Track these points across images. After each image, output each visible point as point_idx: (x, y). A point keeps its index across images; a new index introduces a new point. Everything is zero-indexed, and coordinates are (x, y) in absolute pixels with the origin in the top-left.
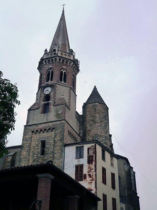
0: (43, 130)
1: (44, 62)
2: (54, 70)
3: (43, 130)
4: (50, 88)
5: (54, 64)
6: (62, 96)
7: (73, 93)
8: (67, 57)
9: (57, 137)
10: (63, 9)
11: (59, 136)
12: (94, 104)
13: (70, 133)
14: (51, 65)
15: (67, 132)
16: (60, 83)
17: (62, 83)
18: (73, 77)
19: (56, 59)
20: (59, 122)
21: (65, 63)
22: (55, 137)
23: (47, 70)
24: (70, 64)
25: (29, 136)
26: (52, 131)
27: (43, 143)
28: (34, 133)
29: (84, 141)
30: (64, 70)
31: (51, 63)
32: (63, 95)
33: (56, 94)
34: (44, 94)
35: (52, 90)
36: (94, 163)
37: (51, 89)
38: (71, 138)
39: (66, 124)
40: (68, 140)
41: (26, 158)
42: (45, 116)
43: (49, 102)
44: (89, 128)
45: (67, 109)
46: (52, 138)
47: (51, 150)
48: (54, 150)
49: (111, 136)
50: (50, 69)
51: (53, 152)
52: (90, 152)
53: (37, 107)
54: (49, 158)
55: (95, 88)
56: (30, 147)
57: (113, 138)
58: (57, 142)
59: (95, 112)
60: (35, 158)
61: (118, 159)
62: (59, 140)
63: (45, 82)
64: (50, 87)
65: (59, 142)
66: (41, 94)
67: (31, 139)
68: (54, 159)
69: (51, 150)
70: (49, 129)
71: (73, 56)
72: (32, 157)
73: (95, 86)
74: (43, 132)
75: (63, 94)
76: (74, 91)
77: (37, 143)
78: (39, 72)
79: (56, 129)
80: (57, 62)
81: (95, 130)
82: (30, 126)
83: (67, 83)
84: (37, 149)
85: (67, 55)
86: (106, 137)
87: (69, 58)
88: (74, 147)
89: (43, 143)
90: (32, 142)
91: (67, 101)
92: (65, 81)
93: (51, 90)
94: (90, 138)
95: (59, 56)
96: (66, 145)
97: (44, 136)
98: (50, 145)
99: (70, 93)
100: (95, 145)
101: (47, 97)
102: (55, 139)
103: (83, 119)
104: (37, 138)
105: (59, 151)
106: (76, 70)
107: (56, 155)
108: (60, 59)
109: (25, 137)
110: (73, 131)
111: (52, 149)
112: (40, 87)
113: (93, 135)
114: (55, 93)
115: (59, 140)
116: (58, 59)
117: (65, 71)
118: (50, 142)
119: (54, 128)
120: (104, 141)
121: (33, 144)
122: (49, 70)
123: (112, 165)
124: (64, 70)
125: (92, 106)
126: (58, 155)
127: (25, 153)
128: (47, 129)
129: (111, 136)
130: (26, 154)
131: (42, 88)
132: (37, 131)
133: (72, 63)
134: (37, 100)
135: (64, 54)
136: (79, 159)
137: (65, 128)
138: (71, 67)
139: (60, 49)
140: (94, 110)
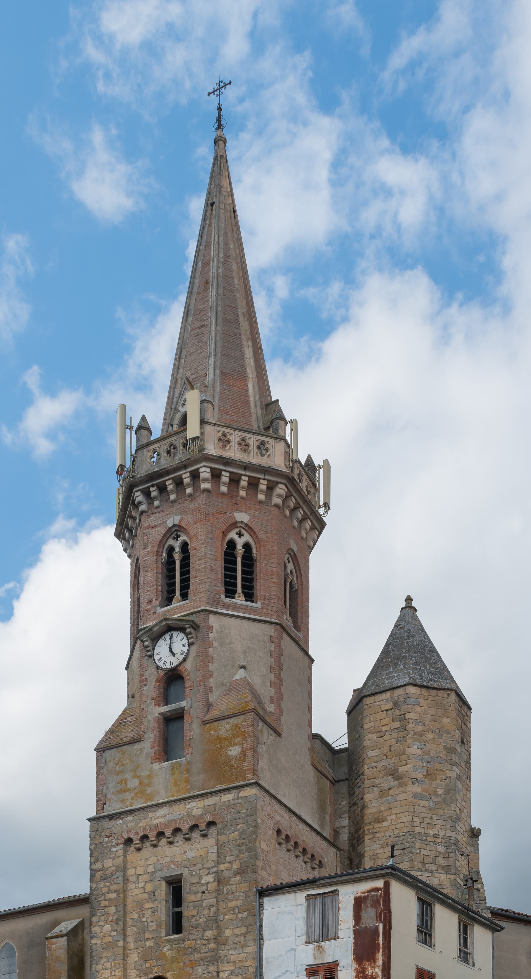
0: (168, 832)
1: (139, 497)
2: (190, 539)
3: (168, 832)
4: (181, 635)
5: (192, 506)
6: (241, 674)
7: (295, 647)
8: (254, 458)
9: (228, 859)
10: (219, 120)
11: (236, 856)
12: (397, 692)
13: (283, 837)
14: (174, 509)
15: (271, 833)
16: (226, 606)
17: (235, 607)
18: (290, 566)
19: (195, 475)
20: (228, 797)
21: (243, 493)
22: (218, 862)
23: (161, 543)
24: (271, 499)
25: (114, 859)
26: (204, 836)
27: (176, 888)
28: (132, 849)
29: (352, 866)
30: (240, 535)
31: (174, 502)
32: (243, 667)
33: (211, 667)
34: (158, 668)
35: (191, 644)
36: (380, 956)
37: (185, 641)
38: (294, 858)
39: (266, 805)
40: (284, 866)
41: (110, 946)
42: (175, 770)
43: (183, 704)
44: (371, 811)
45: (267, 736)
46: (210, 865)
47: (206, 912)
48: (216, 914)
49: (475, 834)
50: (175, 531)
51: (216, 921)
52: (364, 915)
53: (132, 735)
54: (204, 942)
55: (409, 606)
56: (125, 905)
57: (484, 843)
58: (229, 878)
59: (402, 734)
60: (150, 944)
61: (495, 929)
62: (237, 873)
63: (155, 607)
64: (182, 629)
65: (237, 879)
66: (142, 668)
67: (125, 870)
68: (222, 947)
69: (206, 912)
70: (194, 827)
71: (282, 443)
72: (137, 940)
73: (409, 599)
74: (171, 843)
75: (243, 663)
76: (300, 635)
77: (149, 887)
78: (125, 550)
79: (219, 826)
80: (205, 490)
81: (393, 815)
82: (111, 817)
83: (258, 605)
84: (154, 910)
85: (253, 441)
86: (452, 844)
87: (264, 461)
88: (301, 897)
89: (176, 888)
90: (131, 886)
91: (266, 692)
92: (249, 596)
93: (184, 646)
94: (378, 852)
95: (209, 458)
96: (263, 893)
97: (174, 856)
98: (203, 893)
99: (278, 654)
100: (387, 885)
101: (173, 678)
102: (222, 867)
103: (350, 769)
104: (148, 868)
105: (240, 916)
106: (308, 525)
107: (228, 933)
108: (216, 475)
109: (99, 865)
110: (301, 826)
111: (212, 909)
112: (137, 635)
113: (392, 839)
114: (205, 658)
115: (237, 873)
116: (205, 473)
117: (246, 538)
118: (203, 881)
119: (211, 824)
120: (440, 861)
121: (135, 892)
122: (171, 542)
123: (465, 955)
124: (240, 535)
125: (390, 705)
126: (237, 931)
127: (107, 927)
128: (185, 828)
129: (475, 834)
130: (112, 931)
131: (143, 642)
132: (145, 838)
133: (281, 490)
134: (131, 697)
135: (235, 437)
136: (319, 944)
137: (259, 821)
138: (276, 511)
139: (211, 417)
140: (397, 725)
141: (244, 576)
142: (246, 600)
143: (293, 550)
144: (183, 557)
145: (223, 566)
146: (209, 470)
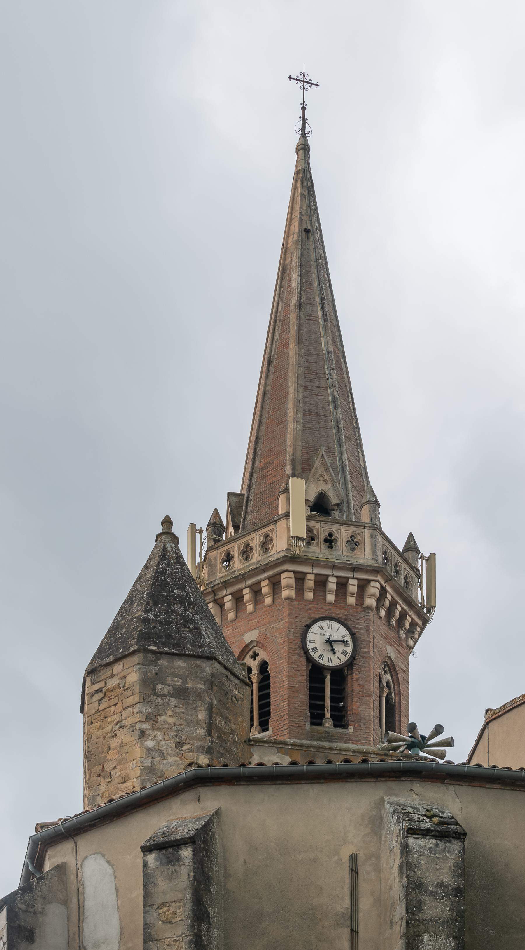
141: (333, 704)
142: (335, 726)
143: (390, 658)
144: (262, 679)
145: (308, 703)
146: (292, 575)
